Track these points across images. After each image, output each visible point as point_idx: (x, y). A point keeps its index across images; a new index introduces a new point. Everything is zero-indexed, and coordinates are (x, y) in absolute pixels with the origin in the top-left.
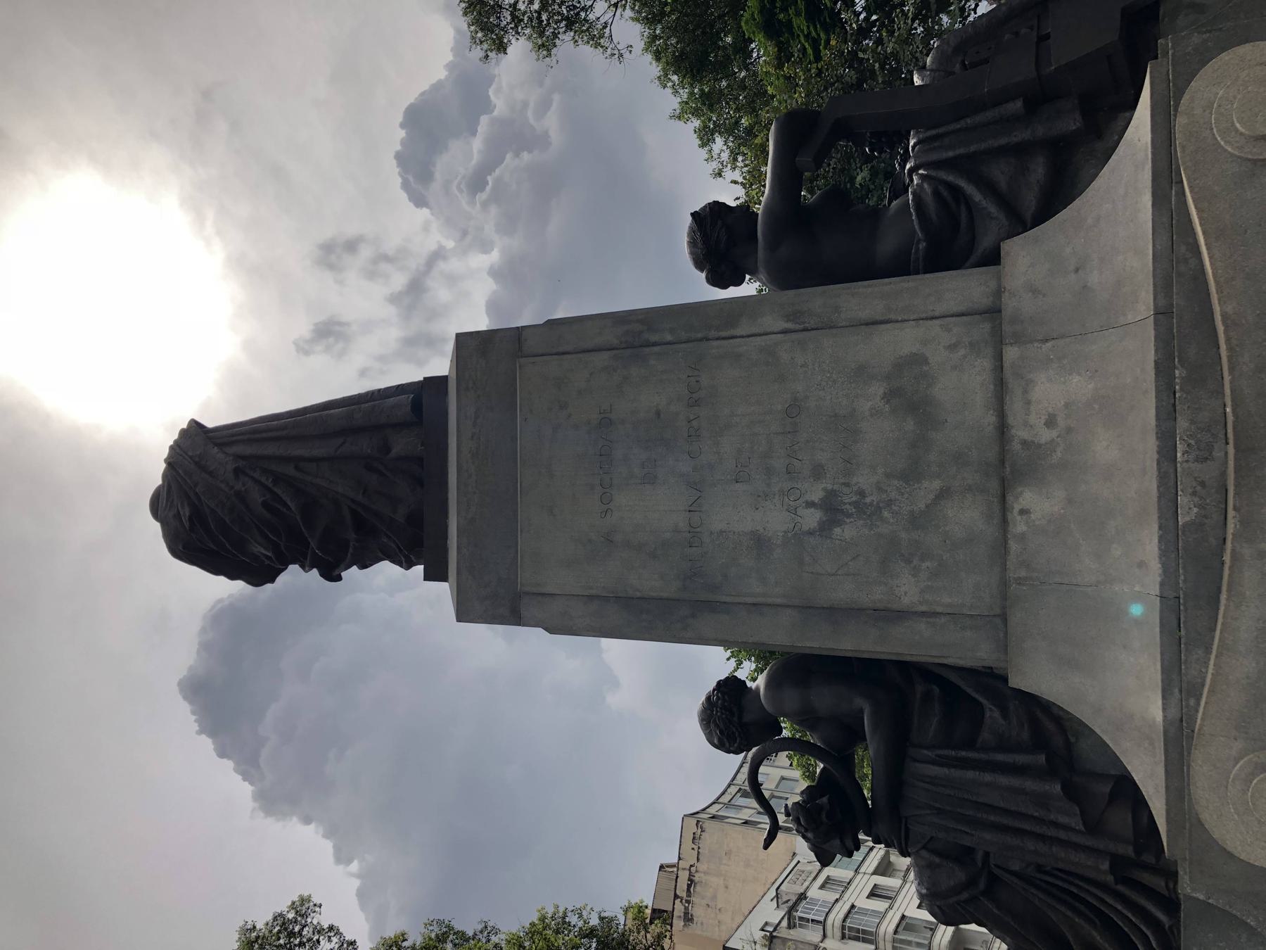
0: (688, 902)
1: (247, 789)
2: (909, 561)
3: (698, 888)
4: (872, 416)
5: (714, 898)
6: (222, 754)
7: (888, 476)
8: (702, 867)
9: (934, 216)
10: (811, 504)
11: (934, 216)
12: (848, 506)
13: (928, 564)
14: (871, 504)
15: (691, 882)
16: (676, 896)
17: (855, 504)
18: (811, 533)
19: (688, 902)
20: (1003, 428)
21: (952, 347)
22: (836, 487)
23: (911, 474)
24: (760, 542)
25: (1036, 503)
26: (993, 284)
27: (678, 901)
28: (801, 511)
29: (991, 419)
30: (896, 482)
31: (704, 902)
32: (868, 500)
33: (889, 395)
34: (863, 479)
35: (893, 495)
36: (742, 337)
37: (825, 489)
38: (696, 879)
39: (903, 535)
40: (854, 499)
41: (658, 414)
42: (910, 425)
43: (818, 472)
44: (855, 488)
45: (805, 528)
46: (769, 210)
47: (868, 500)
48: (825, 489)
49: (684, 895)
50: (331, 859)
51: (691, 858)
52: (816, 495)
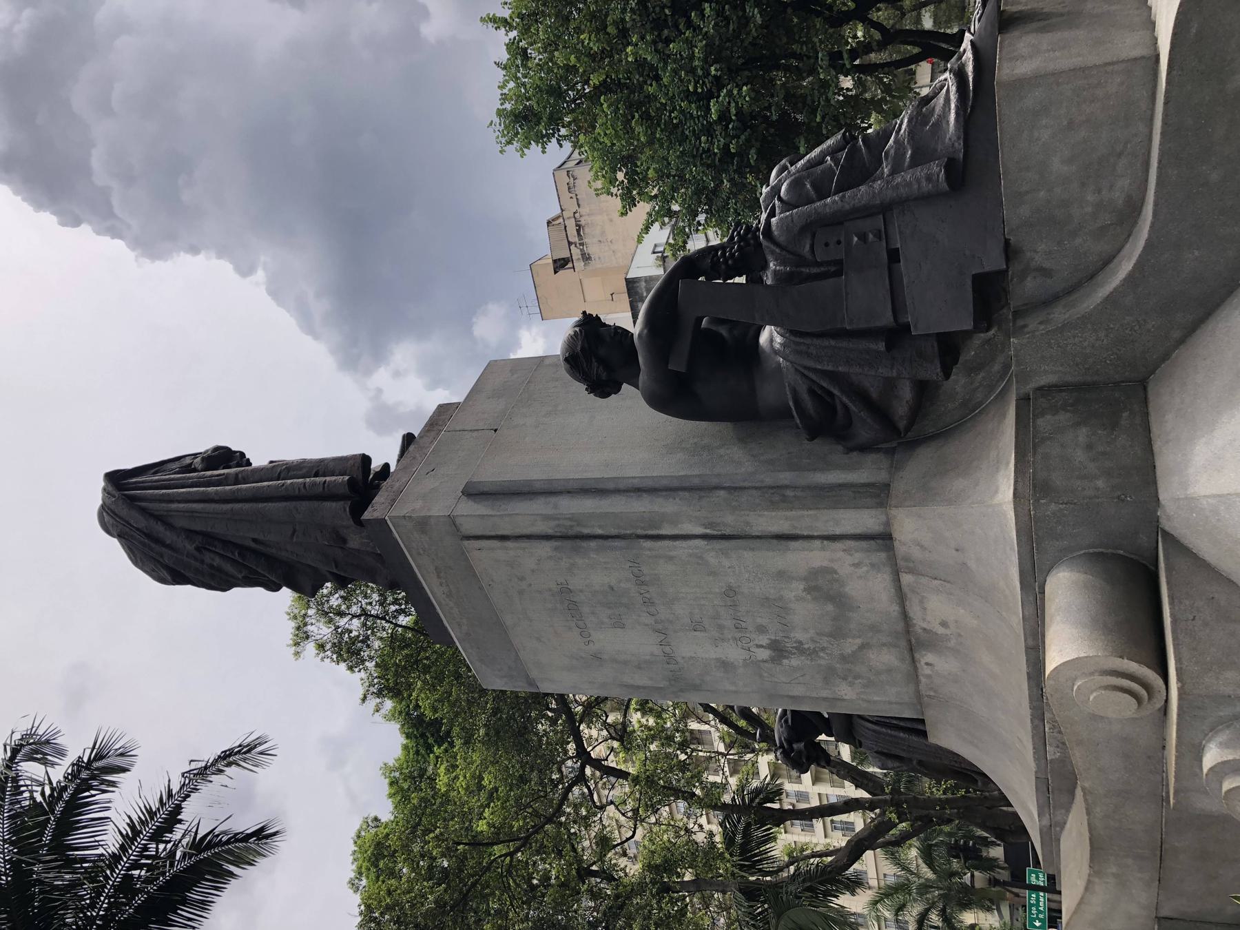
0: (582, 244)
1: (119, 243)
2: (845, 679)
3: (587, 230)
5: (603, 233)
6: (74, 221)
8: (584, 210)
9: (812, 412)
11: (812, 412)
15: (579, 228)
16: (570, 243)
19: (582, 244)
20: (905, 616)
21: (857, 565)
23: (838, 634)
24: (725, 665)
25: (934, 664)
26: (883, 518)
27: (573, 247)
29: (895, 609)
31: (595, 240)
33: (808, 590)
34: (799, 635)
38: (583, 223)
46: (640, 335)
49: (576, 240)
50: (235, 277)
51: (571, 206)
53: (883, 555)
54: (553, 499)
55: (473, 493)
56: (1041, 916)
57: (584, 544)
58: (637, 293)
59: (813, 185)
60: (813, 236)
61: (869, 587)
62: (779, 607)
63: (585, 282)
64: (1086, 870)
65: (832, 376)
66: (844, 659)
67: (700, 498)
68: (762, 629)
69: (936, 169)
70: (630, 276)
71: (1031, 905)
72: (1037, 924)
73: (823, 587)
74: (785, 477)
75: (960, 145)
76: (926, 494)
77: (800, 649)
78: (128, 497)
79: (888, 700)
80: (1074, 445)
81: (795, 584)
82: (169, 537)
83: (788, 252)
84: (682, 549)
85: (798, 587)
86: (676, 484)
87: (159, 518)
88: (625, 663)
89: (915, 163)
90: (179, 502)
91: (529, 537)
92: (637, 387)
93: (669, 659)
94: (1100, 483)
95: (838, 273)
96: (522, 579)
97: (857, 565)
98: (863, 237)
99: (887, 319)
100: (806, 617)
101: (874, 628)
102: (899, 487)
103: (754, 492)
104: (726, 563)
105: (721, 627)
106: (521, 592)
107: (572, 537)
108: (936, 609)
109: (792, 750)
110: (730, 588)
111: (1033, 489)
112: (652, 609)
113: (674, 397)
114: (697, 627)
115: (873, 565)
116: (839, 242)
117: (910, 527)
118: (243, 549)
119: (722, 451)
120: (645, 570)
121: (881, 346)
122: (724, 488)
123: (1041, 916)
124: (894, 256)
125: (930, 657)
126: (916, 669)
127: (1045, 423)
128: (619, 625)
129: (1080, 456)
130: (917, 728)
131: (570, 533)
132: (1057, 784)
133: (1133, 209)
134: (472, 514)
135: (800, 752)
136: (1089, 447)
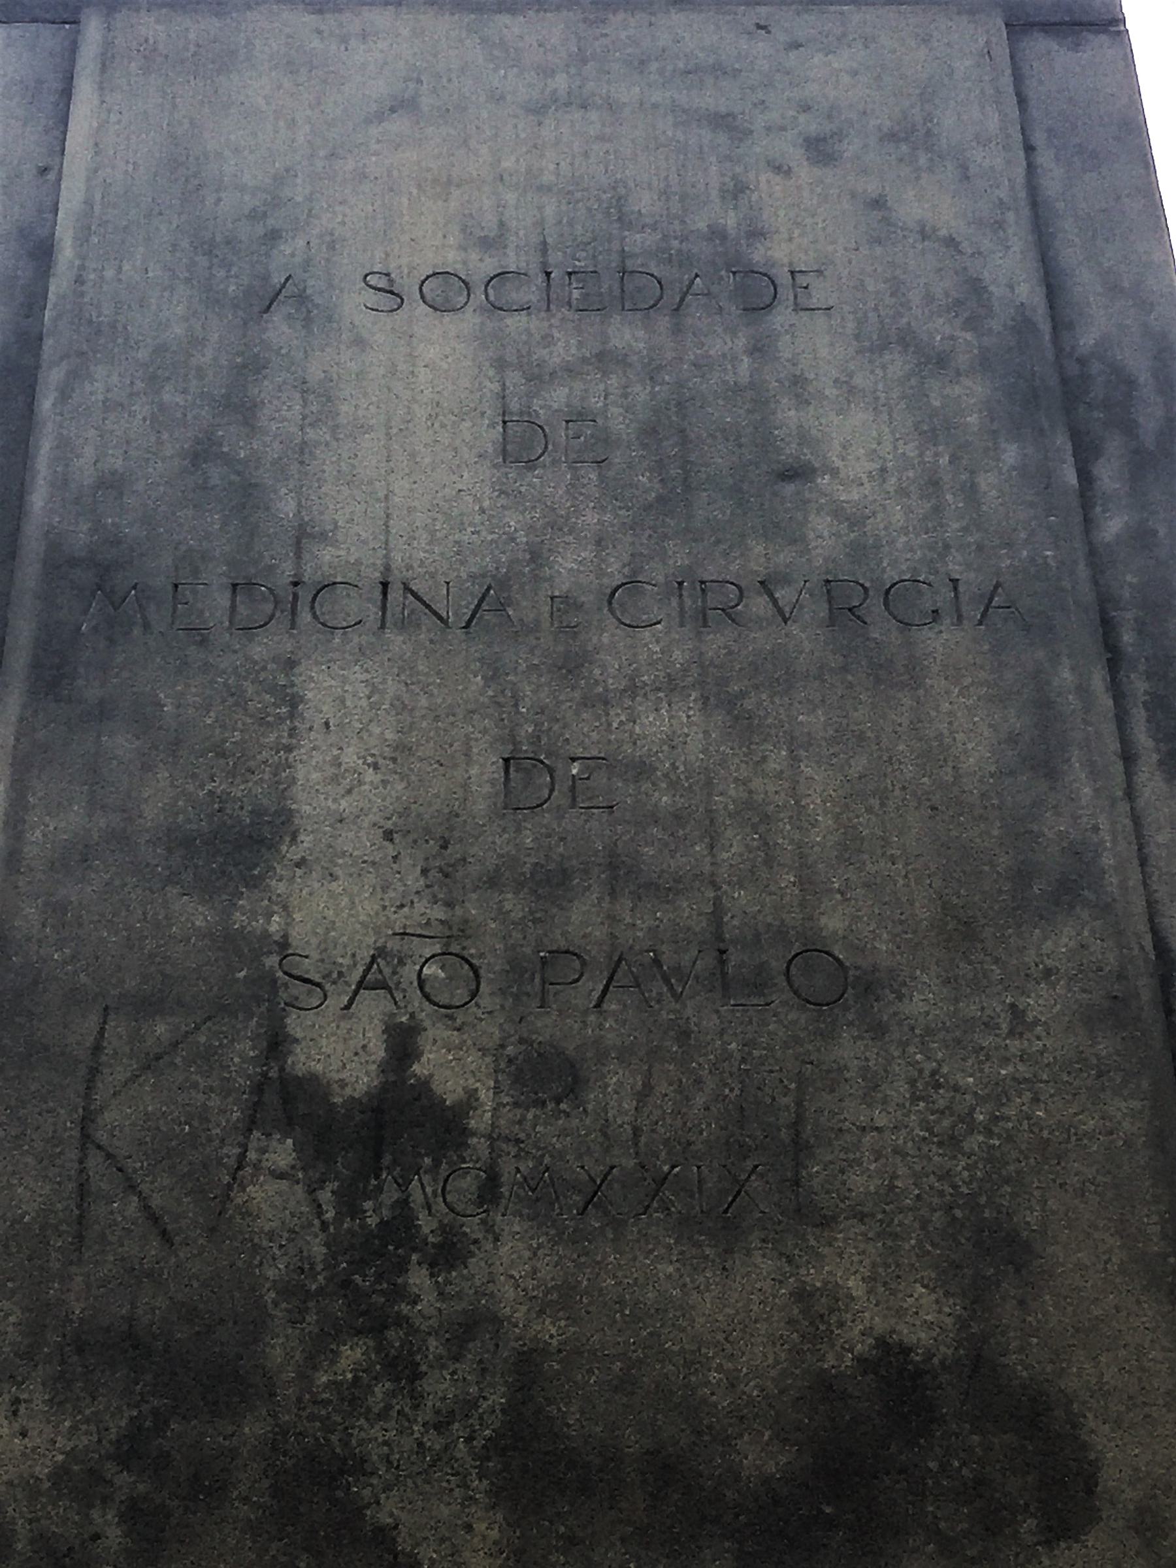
2: (131, 1450)
4: (802, 1295)
7: (528, 1365)
10: (403, 1044)
12: (390, 1195)
13: (114, 1535)
14: (398, 1293)
17: (401, 1224)
18: (277, 1044)
22: (479, 1145)
28: (373, 1006)
30: (497, 1398)
32: (418, 1278)
34: (512, 1262)
35: (439, 1387)
36: (1130, 794)
37: (471, 1099)
39: (253, 1429)
40: (426, 1224)
41: (796, 474)
42: (760, 1458)
43: (547, 1076)
44: (472, 1227)
45: (295, 1024)
47: (418, 1278)
48: (471, 1099)
52: (452, 1067)
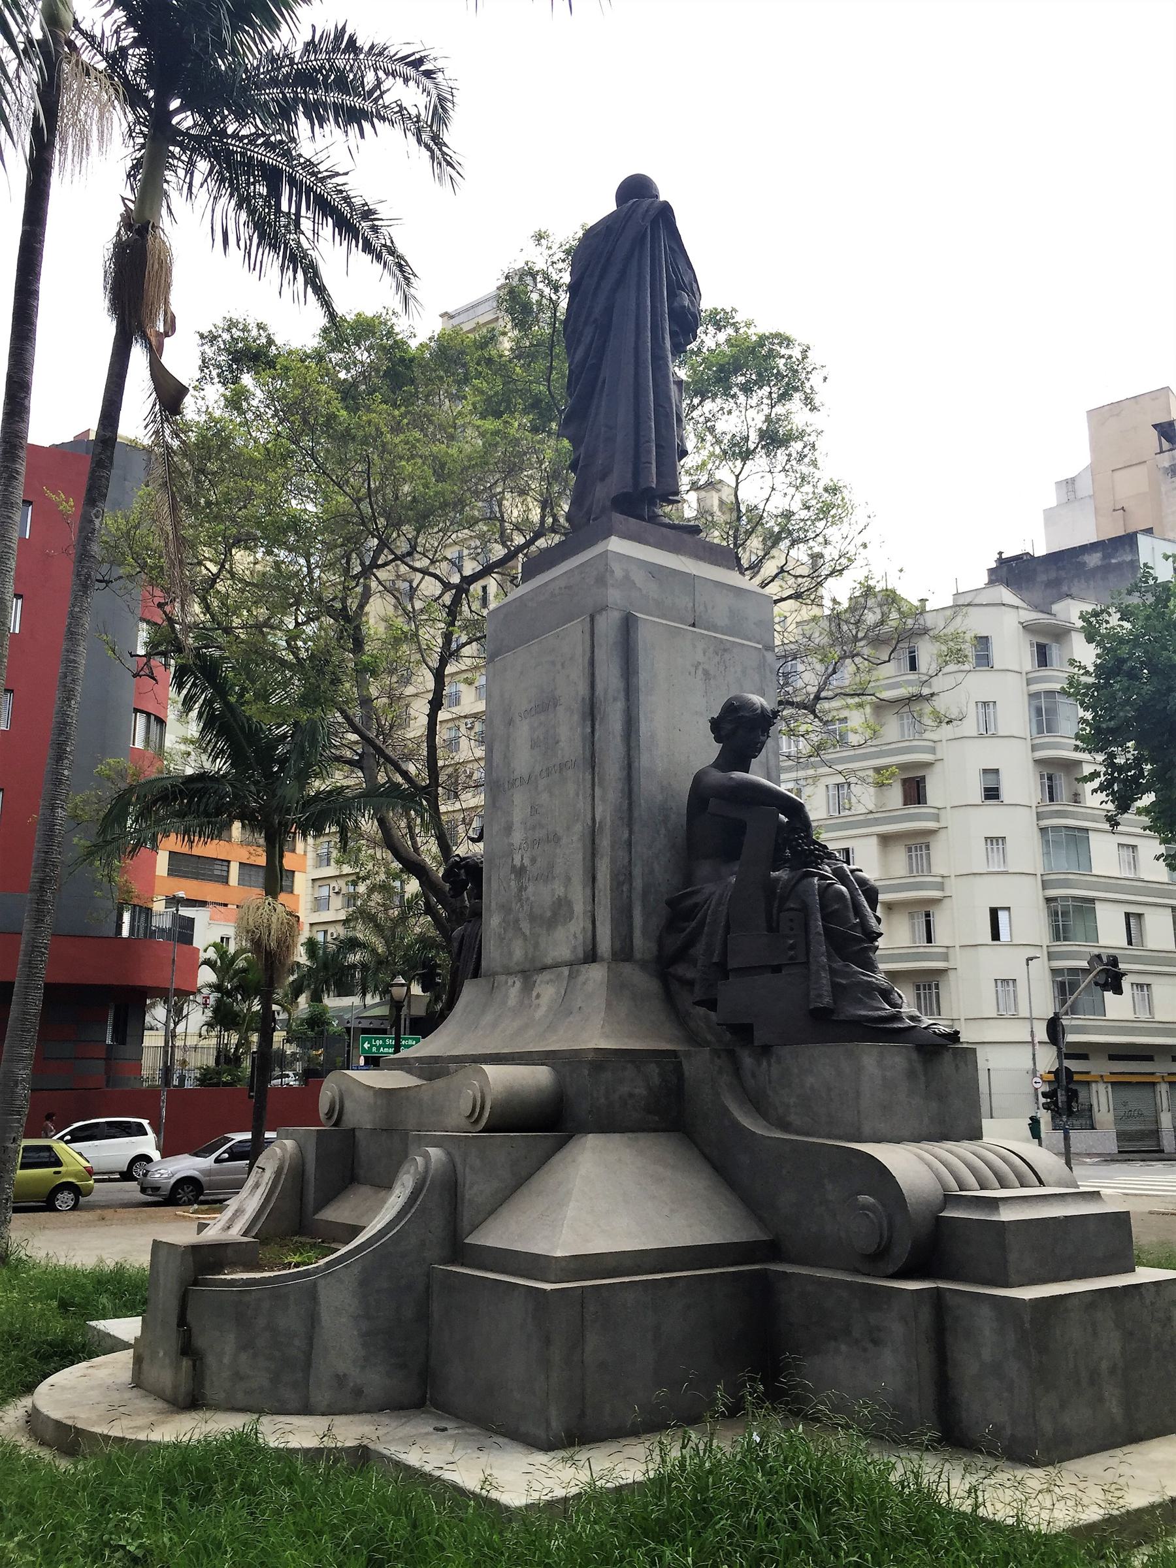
2: (504, 921)
20: (544, 968)
21: (575, 937)
23: (532, 918)
24: (508, 829)
29: (549, 961)
53: (581, 955)
54: (622, 695)
55: (628, 624)
56: (374, 1049)
57: (589, 723)
58: (1116, 550)
59: (837, 910)
60: (800, 911)
61: (563, 943)
62: (547, 876)
63: (1143, 469)
64: (378, 1086)
65: (702, 923)
66: (517, 921)
67: (621, 818)
68: (533, 860)
69: (827, 1000)
70: (1142, 540)
71: (384, 1040)
72: (366, 1045)
73: (560, 911)
74: (638, 883)
75: (842, 1017)
76: (616, 987)
77: (522, 889)
78: (644, 236)
79: (492, 954)
80: (634, 1086)
81: (562, 889)
82: (607, 285)
83: (792, 887)
84: (582, 805)
85: (560, 891)
86: (634, 798)
87: (623, 273)
88: (508, 746)
89: (835, 986)
90: (638, 298)
91: (593, 675)
92: (711, 766)
93: (512, 784)
94: (602, 1100)
95: (770, 929)
96: (563, 665)
97: (575, 937)
98: (792, 947)
99: (732, 964)
100: (542, 894)
101: (536, 946)
102: (627, 969)
103: (627, 860)
104: (575, 838)
105: (534, 828)
106: (553, 663)
107: (591, 712)
108: (547, 991)
109: (459, 869)
110: (559, 839)
111: (603, 1060)
112: (544, 774)
113: (701, 793)
114: (534, 810)
115: (575, 947)
116: (792, 929)
117: (596, 974)
118: (597, 367)
119: (663, 831)
120: (570, 773)
121: (715, 960)
122: (630, 836)
123: (374, 1049)
124: (777, 969)
125: (518, 984)
126: (511, 974)
127: (653, 1070)
128: (534, 745)
129: (624, 1089)
130: (476, 974)
131: (596, 711)
132: (432, 1068)
133: (785, 1127)
134: (608, 624)
135: (458, 875)
136: (631, 1095)
